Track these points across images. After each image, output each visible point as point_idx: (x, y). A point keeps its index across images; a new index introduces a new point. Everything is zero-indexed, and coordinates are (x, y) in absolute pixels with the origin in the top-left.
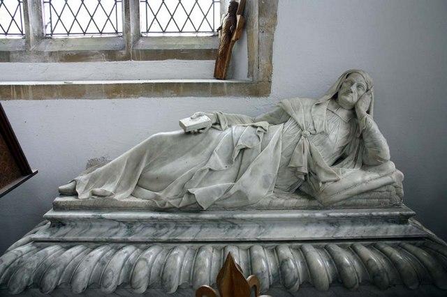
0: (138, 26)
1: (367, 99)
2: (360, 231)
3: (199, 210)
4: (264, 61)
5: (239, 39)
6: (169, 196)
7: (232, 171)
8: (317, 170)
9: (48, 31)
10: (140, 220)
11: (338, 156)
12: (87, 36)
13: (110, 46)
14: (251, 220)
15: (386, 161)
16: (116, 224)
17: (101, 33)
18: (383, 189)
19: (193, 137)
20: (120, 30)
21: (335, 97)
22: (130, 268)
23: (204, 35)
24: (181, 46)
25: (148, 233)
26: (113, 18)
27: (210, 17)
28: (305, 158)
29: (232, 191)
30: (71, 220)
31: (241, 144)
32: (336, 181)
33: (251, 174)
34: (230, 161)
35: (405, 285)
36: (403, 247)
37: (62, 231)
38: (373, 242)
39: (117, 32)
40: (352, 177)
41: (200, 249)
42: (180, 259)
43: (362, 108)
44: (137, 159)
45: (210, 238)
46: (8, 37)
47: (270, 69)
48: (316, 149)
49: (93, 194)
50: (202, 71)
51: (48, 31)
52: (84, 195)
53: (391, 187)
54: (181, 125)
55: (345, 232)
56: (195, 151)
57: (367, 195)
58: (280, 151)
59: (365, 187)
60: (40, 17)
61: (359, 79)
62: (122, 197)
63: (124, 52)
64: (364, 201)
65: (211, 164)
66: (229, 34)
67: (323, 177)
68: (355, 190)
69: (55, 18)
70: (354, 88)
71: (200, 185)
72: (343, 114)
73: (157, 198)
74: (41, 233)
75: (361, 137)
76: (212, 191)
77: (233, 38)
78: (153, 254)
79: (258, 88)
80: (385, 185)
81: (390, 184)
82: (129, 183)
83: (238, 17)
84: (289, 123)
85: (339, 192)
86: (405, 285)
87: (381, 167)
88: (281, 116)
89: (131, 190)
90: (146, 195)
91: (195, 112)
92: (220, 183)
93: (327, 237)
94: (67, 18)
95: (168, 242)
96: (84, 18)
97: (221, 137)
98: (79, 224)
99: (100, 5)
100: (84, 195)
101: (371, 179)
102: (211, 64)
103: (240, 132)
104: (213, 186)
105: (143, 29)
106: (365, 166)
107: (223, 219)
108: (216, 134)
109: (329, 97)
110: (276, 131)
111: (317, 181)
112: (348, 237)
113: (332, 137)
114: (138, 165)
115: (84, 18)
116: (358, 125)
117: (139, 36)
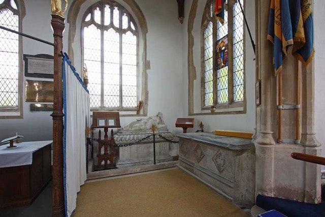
6: (137, 128)
25: (134, 133)
40: (160, 126)
50: (135, 113)
62: (130, 129)
79: (145, 115)
91: (138, 118)
102: (136, 112)
106: (302, 134)
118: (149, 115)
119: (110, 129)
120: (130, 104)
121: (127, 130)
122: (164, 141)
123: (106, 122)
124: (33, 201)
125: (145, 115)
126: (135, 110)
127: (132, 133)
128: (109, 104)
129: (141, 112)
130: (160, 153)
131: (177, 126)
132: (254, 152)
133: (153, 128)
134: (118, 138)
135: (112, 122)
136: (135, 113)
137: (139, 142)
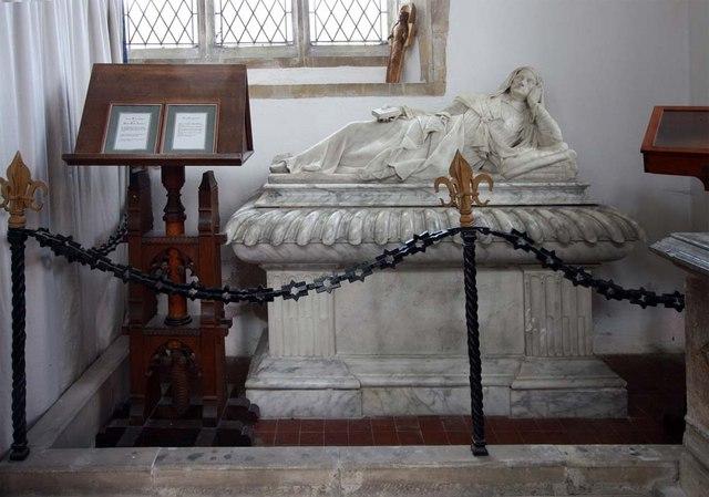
0: (308, 36)
1: (538, 91)
2: (540, 198)
3: (400, 181)
4: (438, 64)
5: (411, 47)
6: (372, 170)
7: (424, 150)
8: (498, 149)
9: (218, 40)
10: (348, 189)
11: (514, 141)
12: (256, 45)
13: (283, 54)
14: (347, 182)
15: (559, 141)
16: (327, 193)
17: (270, 42)
18: (558, 164)
19: (384, 125)
20: (290, 39)
21: (508, 91)
22: (346, 225)
23: (372, 44)
24: (352, 53)
25: (356, 200)
26: (282, 28)
27: (377, 27)
28: (486, 140)
29: (425, 165)
30: (286, 190)
31: (429, 128)
32: (515, 157)
33: (440, 152)
34: (420, 143)
35: (586, 242)
36: (315, 188)
37: (279, 199)
38: (555, 207)
39: (286, 41)
40: (528, 155)
41: (402, 212)
42: (384, 217)
43: (533, 99)
44: (337, 143)
45: (410, 204)
46: (179, 46)
47: (445, 70)
48: (494, 132)
49: (304, 170)
50: (377, 74)
51: (218, 40)
52: (296, 172)
53: (565, 163)
54: (374, 113)
55: (527, 198)
56: (387, 136)
57: (544, 170)
58: (463, 134)
59: (541, 162)
60: (213, 27)
61: (529, 74)
62: (329, 172)
63: (298, 60)
64: (542, 175)
65: (404, 144)
66: (401, 41)
67: (503, 154)
68: (533, 164)
69: (226, 28)
70: (524, 82)
71: (396, 161)
72: (517, 104)
73: (361, 172)
74: (262, 202)
75: (535, 122)
76: (409, 165)
77: (406, 44)
78: (335, 217)
79: (432, 87)
80: (560, 161)
81: (564, 160)
82: (332, 161)
83: (410, 25)
84: (469, 112)
85: (519, 166)
86: (586, 242)
87: (556, 146)
88: (461, 107)
89: (335, 167)
90: (350, 171)
91: (386, 105)
92: (414, 159)
93: (512, 203)
94: (238, 28)
95: (374, 206)
96: (254, 28)
97: (409, 125)
98: (283, 194)
99: (168, 24)
100: (296, 172)
101: (547, 156)
102: (384, 69)
103: (429, 121)
104: (408, 162)
105: (313, 39)
106: (539, 146)
107: (420, 189)
108: (404, 123)
109: (503, 91)
110: (457, 119)
111: (499, 158)
112: (530, 203)
113: (508, 123)
114: (338, 148)
115: (254, 28)
116: (531, 113)
117: (310, 44)
118: (456, 86)
119: (194, 174)
120: (348, 27)
121: (311, 178)
122: (595, 262)
123: (161, 130)
124: (564, 464)
125: (432, 87)
126: (375, 61)
127: (338, 199)
128: (332, 27)
129: (413, 68)
130: (528, 336)
131: (656, 160)
132: (13, 459)
133: (462, 178)
134: (249, 224)
135: (191, 132)
136: (377, 74)
137: (393, 260)
